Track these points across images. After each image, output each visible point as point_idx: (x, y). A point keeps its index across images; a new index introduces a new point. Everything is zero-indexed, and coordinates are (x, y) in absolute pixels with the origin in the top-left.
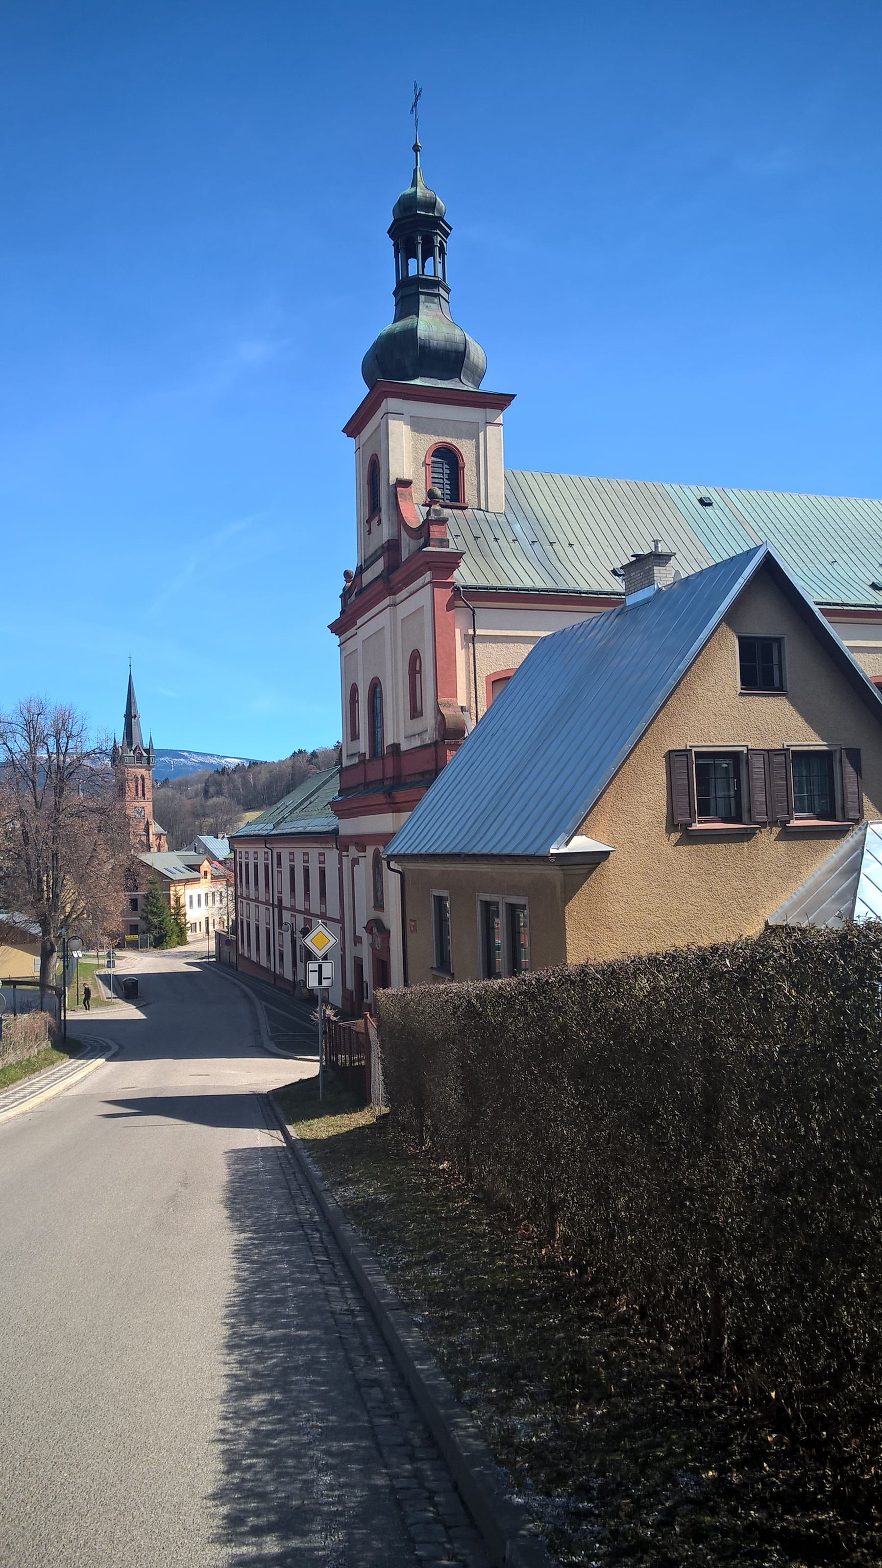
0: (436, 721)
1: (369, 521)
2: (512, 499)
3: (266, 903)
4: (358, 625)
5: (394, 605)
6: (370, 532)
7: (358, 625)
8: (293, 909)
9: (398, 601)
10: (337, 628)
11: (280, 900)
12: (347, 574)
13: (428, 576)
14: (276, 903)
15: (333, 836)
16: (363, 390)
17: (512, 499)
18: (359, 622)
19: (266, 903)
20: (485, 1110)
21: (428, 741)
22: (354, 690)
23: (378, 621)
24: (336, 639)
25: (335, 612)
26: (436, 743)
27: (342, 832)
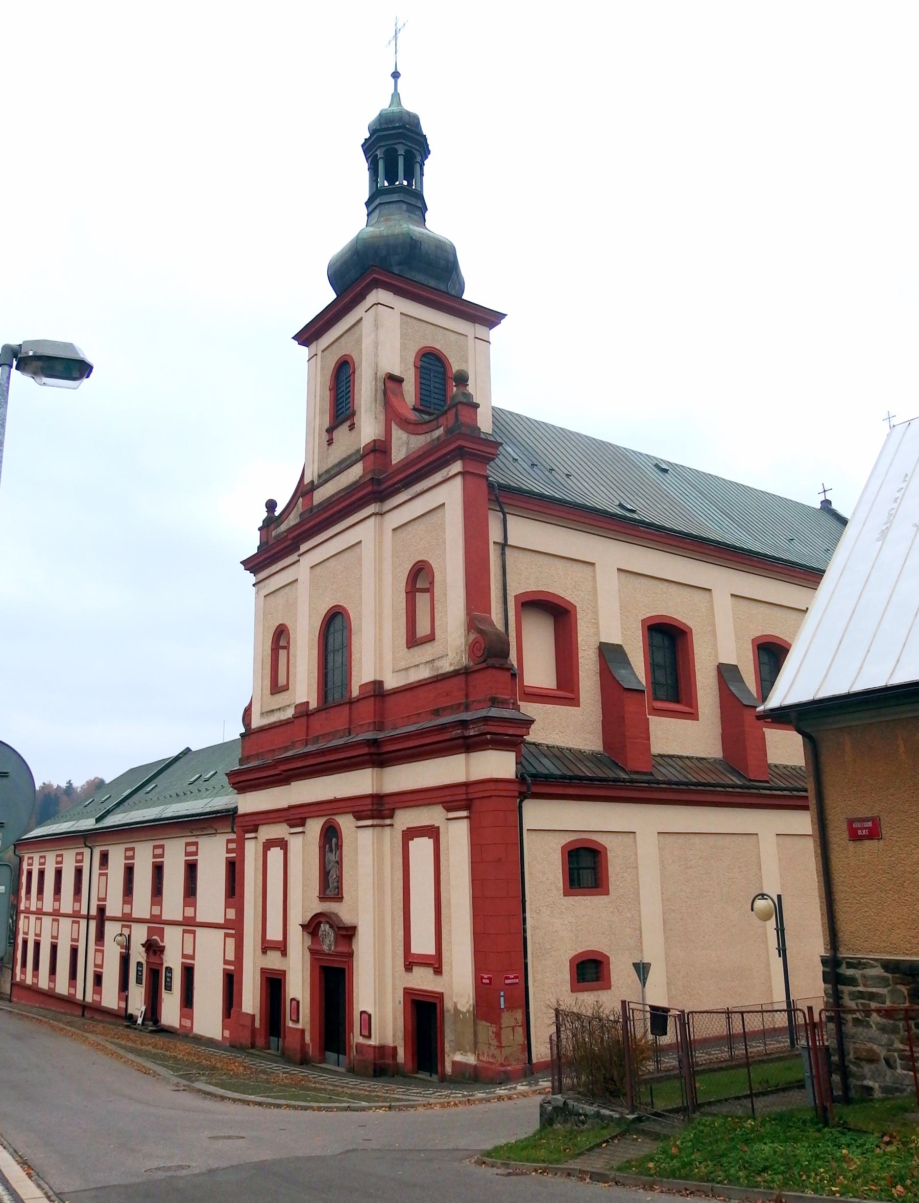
0: (467, 641)
1: (330, 431)
2: (496, 422)
3: (75, 916)
4: (301, 551)
5: (381, 514)
6: (330, 442)
7: (301, 551)
8: (127, 919)
9: (385, 510)
10: (253, 565)
11: (102, 910)
12: (271, 505)
13: (457, 467)
14: (94, 912)
15: (226, 818)
16: (329, 295)
17: (496, 422)
18: (304, 547)
19: (75, 916)
20: (579, 1078)
21: (446, 666)
22: (280, 638)
23: (301, 569)
24: (251, 578)
25: (251, 545)
26: (463, 673)
27: (241, 811)
